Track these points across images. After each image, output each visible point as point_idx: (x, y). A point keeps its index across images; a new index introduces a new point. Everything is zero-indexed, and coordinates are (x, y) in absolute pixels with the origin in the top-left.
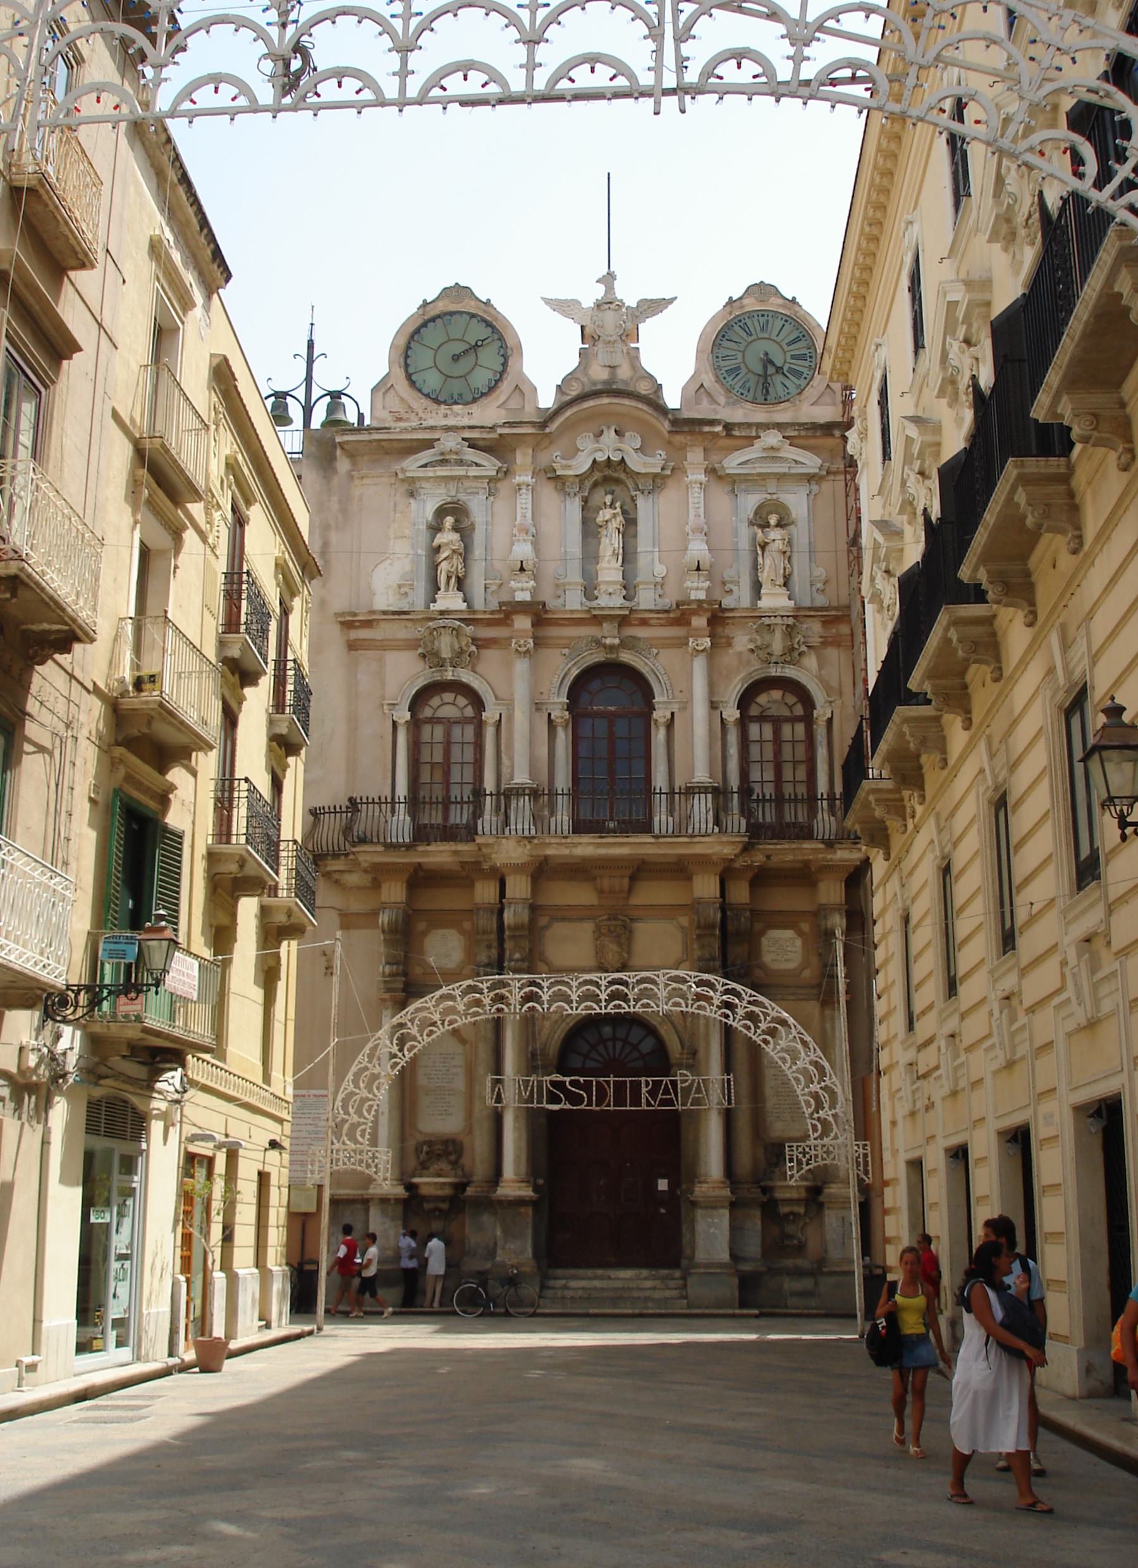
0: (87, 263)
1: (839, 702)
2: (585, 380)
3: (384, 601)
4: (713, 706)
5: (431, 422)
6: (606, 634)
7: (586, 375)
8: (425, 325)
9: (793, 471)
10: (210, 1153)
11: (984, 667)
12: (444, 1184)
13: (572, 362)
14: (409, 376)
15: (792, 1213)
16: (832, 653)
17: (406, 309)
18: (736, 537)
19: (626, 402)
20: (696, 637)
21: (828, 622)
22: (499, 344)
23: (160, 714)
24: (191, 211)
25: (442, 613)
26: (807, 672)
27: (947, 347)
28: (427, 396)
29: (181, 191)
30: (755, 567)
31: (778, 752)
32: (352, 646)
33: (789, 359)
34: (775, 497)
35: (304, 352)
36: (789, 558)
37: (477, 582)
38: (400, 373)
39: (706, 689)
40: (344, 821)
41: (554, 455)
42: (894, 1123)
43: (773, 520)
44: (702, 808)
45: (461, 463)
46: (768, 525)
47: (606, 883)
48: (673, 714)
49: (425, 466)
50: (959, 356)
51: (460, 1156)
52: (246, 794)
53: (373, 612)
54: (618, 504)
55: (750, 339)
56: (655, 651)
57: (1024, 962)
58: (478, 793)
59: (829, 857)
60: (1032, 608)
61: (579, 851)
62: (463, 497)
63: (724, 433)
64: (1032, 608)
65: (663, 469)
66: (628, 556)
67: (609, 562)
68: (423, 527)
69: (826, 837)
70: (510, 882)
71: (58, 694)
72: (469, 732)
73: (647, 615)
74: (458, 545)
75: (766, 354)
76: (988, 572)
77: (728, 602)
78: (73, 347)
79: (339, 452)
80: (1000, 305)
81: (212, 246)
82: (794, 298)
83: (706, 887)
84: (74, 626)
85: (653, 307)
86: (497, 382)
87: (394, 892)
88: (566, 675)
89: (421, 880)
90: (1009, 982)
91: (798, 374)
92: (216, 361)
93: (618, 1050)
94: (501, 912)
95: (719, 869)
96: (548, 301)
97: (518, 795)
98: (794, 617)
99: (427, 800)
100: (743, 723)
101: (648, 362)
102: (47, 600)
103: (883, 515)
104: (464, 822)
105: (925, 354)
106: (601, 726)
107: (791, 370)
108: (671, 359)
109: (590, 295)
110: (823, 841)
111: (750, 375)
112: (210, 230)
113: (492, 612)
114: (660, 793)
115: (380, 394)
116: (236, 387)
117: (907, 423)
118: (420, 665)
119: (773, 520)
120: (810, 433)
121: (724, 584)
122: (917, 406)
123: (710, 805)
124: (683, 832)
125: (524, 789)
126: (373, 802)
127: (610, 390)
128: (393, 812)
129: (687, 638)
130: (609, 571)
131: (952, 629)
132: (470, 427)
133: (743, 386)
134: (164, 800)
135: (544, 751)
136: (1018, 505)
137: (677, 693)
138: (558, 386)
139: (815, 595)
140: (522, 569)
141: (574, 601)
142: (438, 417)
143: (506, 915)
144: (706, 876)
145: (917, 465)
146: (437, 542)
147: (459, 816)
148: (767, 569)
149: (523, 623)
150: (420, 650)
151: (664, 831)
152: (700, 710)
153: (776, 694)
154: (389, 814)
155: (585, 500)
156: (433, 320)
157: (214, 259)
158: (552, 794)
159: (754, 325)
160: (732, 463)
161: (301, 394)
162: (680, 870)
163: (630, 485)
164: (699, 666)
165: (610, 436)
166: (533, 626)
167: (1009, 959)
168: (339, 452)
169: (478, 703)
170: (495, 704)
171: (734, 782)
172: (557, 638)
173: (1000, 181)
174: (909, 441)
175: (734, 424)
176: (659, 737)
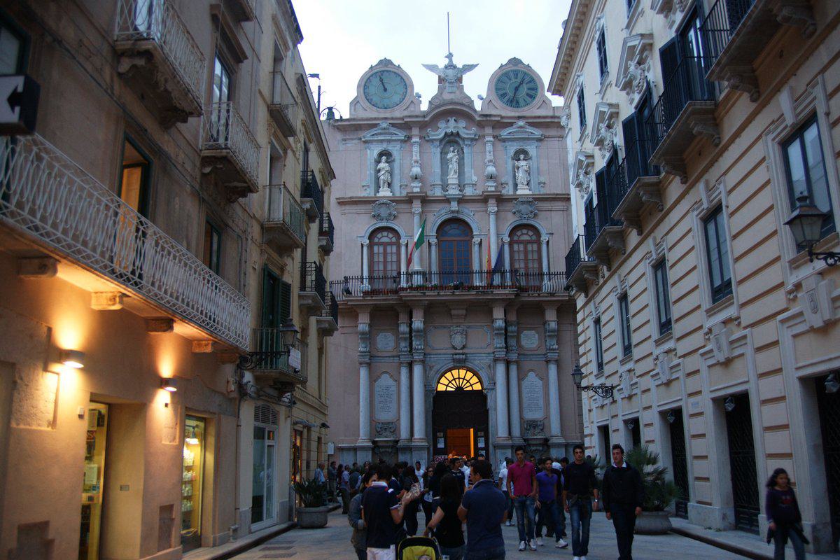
2: (440, 98)
4: (498, 235)
10: (301, 429)
13: (435, 92)
17: (363, 69)
43: (522, 157)
49: (373, 135)
66: (461, 173)
74: (388, 169)
78: (246, 58)
92: (298, 76)
93: (453, 386)
96: (424, 65)
108: (476, 88)
109: (443, 63)
113: (403, 197)
122: (602, 99)
127: (452, 108)
130: (452, 179)
134: (282, 269)
140: (416, 178)
141: (438, 192)
152: (493, 239)
158: (430, 273)
160: (504, 133)
163: (461, 142)
165: (452, 121)
176: (475, 249)
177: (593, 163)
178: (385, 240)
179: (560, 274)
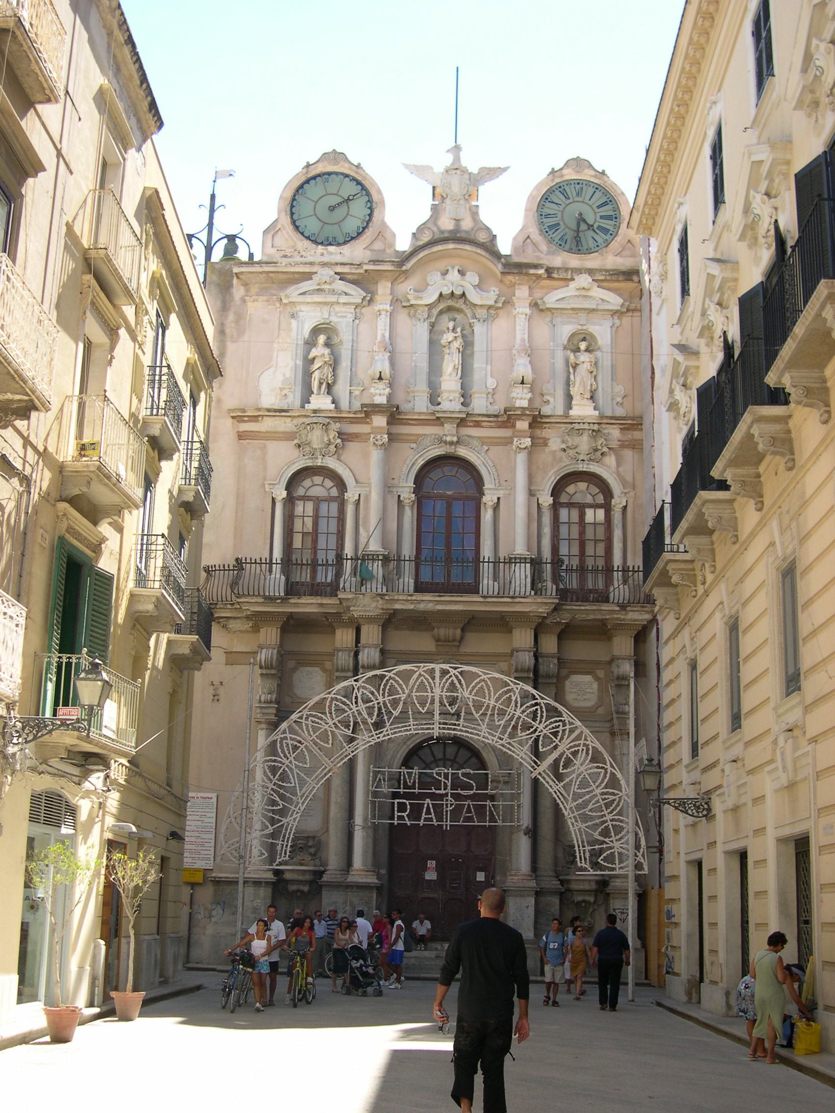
0: (52, 98)
1: (632, 494)
2: (435, 229)
3: (269, 400)
4: (531, 493)
5: (310, 259)
6: (447, 433)
7: (436, 225)
8: (307, 182)
9: (600, 307)
11: (778, 458)
12: (305, 871)
13: (425, 214)
14: (294, 222)
15: (584, 901)
16: (628, 454)
17: (290, 170)
18: (553, 358)
19: (468, 247)
20: (520, 437)
21: (625, 429)
22: (367, 198)
23: (98, 476)
24: (133, 68)
25: (315, 411)
26: (606, 470)
27: (751, 198)
28: (308, 238)
29: (127, 50)
30: (568, 383)
31: (582, 533)
32: (241, 436)
33: (598, 219)
34: (585, 328)
35: (207, 202)
36: (595, 377)
37: (342, 389)
38: (286, 221)
39: (526, 479)
40: (231, 578)
41: (406, 287)
42: (676, 831)
43: (583, 346)
44: (522, 574)
45: (333, 292)
46: (578, 350)
47: (442, 632)
48: (499, 499)
50: (762, 208)
51: (318, 850)
52: (161, 547)
53: (259, 409)
54: (459, 330)
55: (562, 208)
56: (486, 448)
57: (809, 700)
58: (340, 558)
59: (622, 617)
60: (827, 409)
61: (422, 607)
62: (334, 319)
63: (546, 276)
64: (827, 409)
65: (496, 302)
67: (450, 375)
68: (301, 342)
69: (621, 601)
70: (364, 629)
71: (16, 455)
72: (334, 506)
73: (480, 419)
75: (581, 214)
76: (792, 377)
77: (546, 410)
78: (37, 167)
79: (235, 281)
80: (801, 162)
81: (149, 98)
82: (604, 171)
83: (523, 638)
84: (33, 397)
85: (491, 173)
86: (364, 228)
87: (270, 635)
88: (413, 464)
89: (294, 626)
90: (794, 716)
91: (605, 231)
92: (148, 193)
94: (356, 654)
95: (534, 626)
96: (407, 166)
97: (373, 559)
98: (598, 424)
99: (299, 562)
100: (556, 507)
101: (485, 217)
102: (12, 372)
103: (680, 341)
104: (329, 580)
105: (726, 210)
106: (440, 506)
107: (599, 227)
108: (506, 215)
109: (441, 162)
110: (618, 604)
111: (567, 230)
112: (148, 86)
113: (355, 413)
114: (489, 562)
115: (270, 236)
116: (163, 215)
117: (709, 263)
118: (296, 453)
119: (583, 346)
120: (614, 278)
121: (542, 395)
122: (715, 250)
123: (528, 573)
124: (506, 594)
125: (378, 556)
126: (256, 563)
127: (455, 237)
128: (271, 571)
129: (511, 438)
130: (450, 384)
131: (755, 426)
132: (342, 264)
133: (561, 239)
134: (97, 549)
135: (393, 526)
136: (825, 320)
137: (503, 482)
138: (414, 234)
139: (616, 407)
140: (380, 378)
142: (318, 253)
143: (360, 657)
144: (523, 630)
145: (716, 298)
146: (311, 356)
147: (325, 576)
148: (577, 384)
149: (380, 421)
150: (296, 441)
151: (491, 593)
153: (582, 486)
154: (268, 573)
155: (433, 325)
156: (314, 178)
157: (150, 110)
159: (571, 191)
160: (552, 299)
161: (204, 236)
162: (502, 623)
164: (521, 459)
165: (454, 275)
166: (388, 424)
167: (795, 698)
168: (235, 281)
169: (341, 485)
170: (355, 487)
171: (547, 554)
172: (407, 434)
173: (808, 58)
174: (711, 277)
175: (553, 268)
176: (487, 516)
177: (698, 367)
178: (317, 491)
179: (633, 571)
